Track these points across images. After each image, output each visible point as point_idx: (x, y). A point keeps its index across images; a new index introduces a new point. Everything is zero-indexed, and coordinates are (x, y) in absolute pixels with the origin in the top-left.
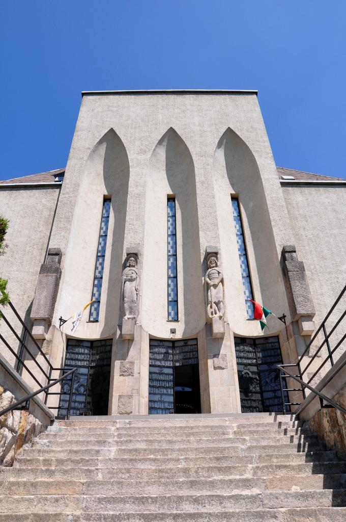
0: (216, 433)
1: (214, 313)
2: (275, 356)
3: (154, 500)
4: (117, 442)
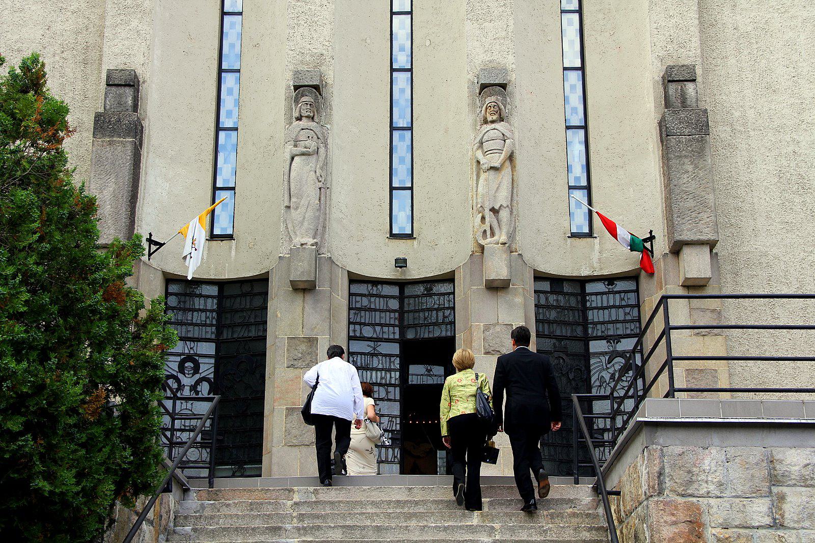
1: (488, 233)
2: (625, 321)
4: (298, 529)
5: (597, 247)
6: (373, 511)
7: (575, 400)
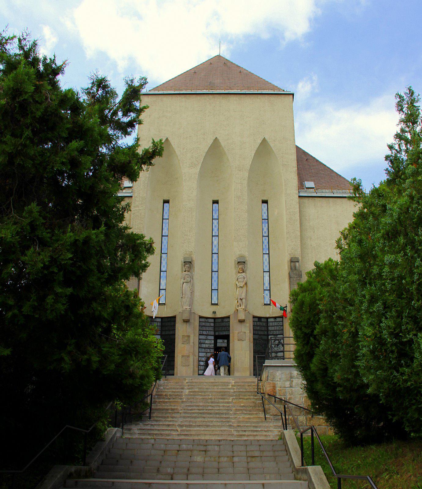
0: (225, 385)
2: (279, 330)
3: (201, 406)
4: (188, 388)
5: (271, 308)
6: (206, 384)
7: (257, 357)
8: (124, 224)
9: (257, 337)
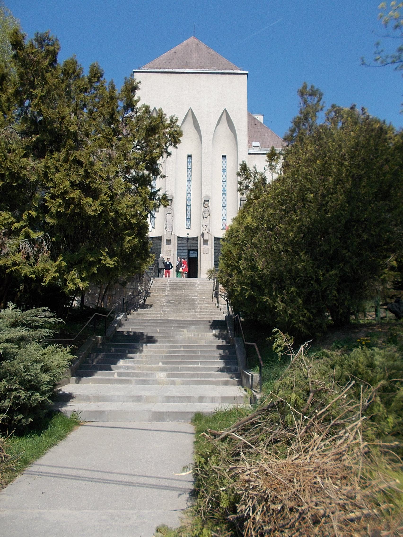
8: (171, 149)
9: (216, 251)
